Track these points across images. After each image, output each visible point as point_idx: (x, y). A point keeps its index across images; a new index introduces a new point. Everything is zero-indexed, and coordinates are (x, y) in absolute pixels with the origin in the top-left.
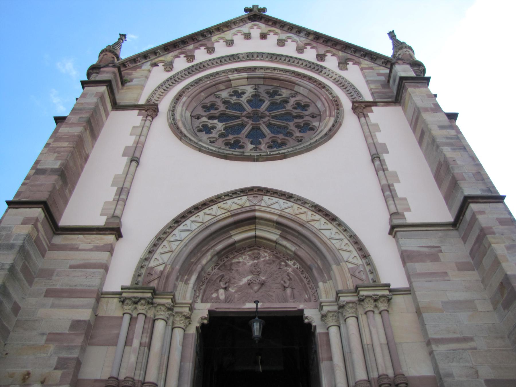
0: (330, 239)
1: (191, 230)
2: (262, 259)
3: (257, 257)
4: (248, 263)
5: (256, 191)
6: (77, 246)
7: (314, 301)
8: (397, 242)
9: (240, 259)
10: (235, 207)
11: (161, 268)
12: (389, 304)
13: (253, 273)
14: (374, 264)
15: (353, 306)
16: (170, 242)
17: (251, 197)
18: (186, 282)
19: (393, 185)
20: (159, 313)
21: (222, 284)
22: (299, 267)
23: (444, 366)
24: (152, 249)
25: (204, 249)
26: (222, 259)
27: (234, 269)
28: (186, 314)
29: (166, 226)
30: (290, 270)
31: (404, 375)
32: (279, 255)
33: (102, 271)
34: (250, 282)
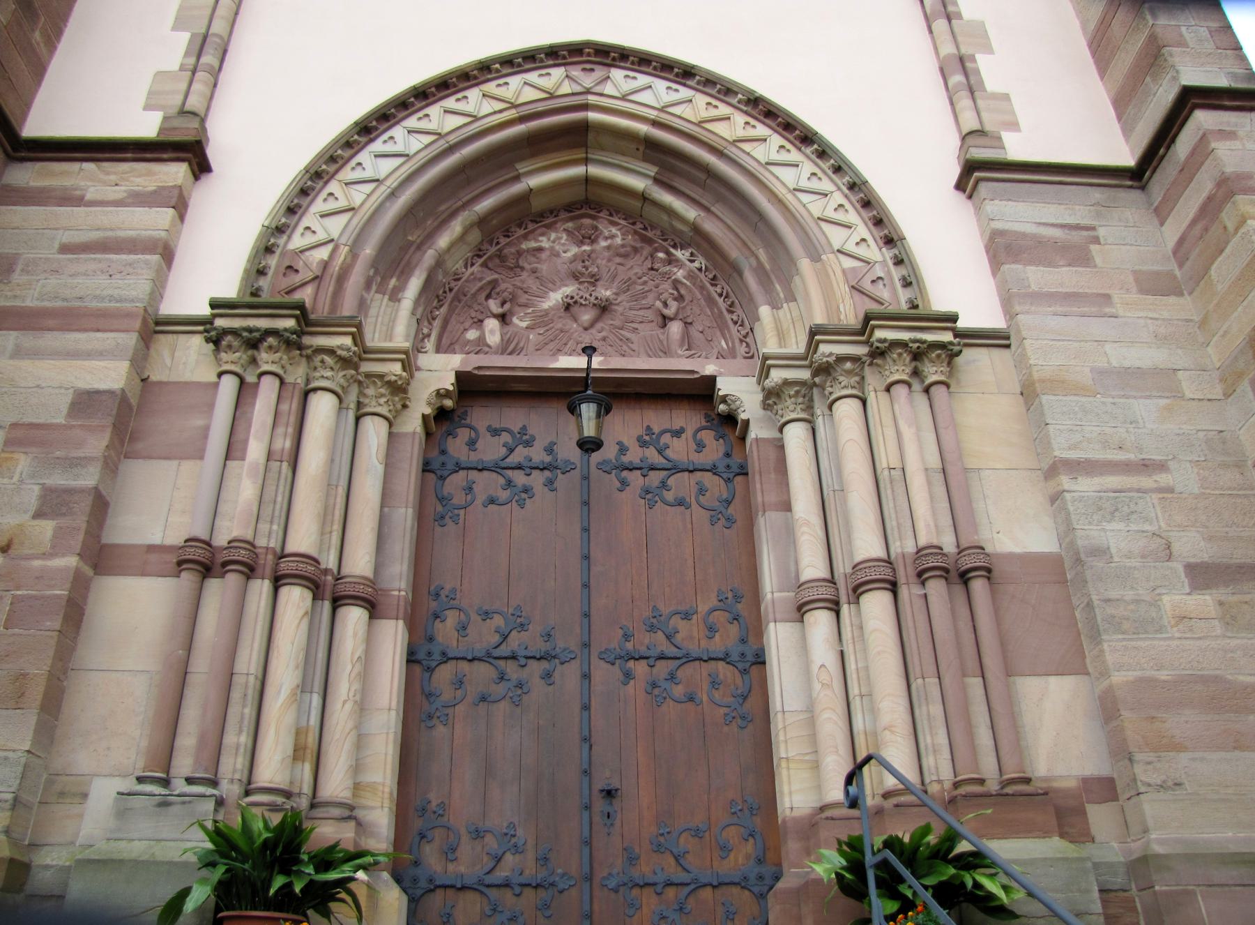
1: (407, 152)
2: (604, 244)
3: (590, 238)
4: (565, 252)
5: (589, 55)
6: (78, 193)
8: (978, 209)
9: (541, 241)
10: (530, 95)
11: (323, 253)
12: (952, 368)
13: (577, 280)
14: (915, 260)
15: (854, 370)
16: (346, 184)
18: (395, 297)
19: (973, 59)
20: (317, 374)
21: (494, 306)
23: (1090, 532)
24: (296, 201)
25: (443, 208)
27: (527, 266)
28: (394, 378)
29: (319, 156)
30: (680, 274)
31: (983, 549)
32: (650, 234)
33: (155, 258)
34: (571, 302)
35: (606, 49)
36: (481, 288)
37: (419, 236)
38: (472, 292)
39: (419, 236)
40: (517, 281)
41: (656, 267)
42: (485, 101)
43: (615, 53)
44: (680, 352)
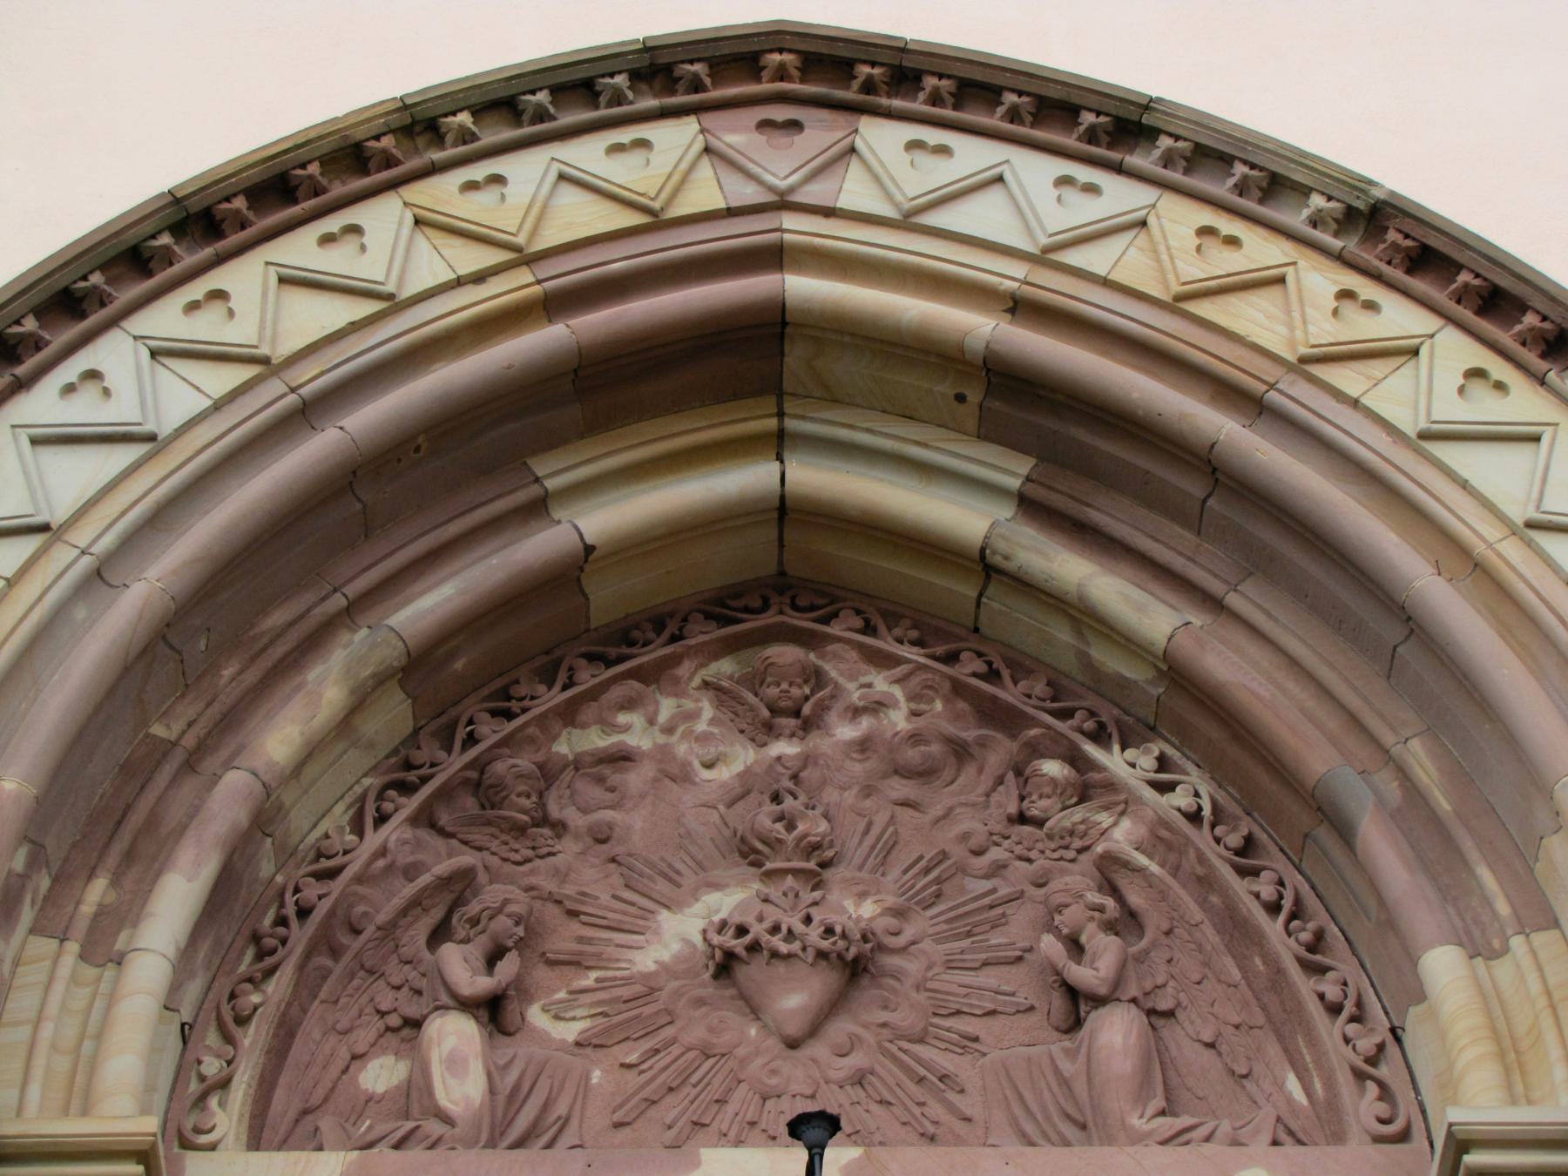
0: (1530, 525)
1: (149, 427)
2: (846, 732)
3: (797, 713)
4: (709, 766)
5: (781, 74)
7: (1379, 1139)
9: (626, 729)
13: (757, 864)
17: (734, 131)
22: (1216, 808)
25: (277, 618)
26: (452, 727)
27: (573, 817)
30: (1122, 835)
32: (1009, 694)
34: (738, 945)
35: (745, 48)
36: (415, 903)
37: (190, 724)
38: (382, 918)
39: (190, 724)
40: (542, 875)
41: (1035, 812)
42: (422, 244)
43: (873, 64)
44: (1135, 1121)
